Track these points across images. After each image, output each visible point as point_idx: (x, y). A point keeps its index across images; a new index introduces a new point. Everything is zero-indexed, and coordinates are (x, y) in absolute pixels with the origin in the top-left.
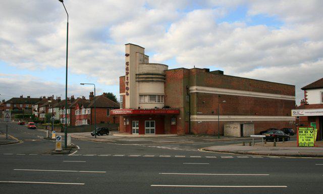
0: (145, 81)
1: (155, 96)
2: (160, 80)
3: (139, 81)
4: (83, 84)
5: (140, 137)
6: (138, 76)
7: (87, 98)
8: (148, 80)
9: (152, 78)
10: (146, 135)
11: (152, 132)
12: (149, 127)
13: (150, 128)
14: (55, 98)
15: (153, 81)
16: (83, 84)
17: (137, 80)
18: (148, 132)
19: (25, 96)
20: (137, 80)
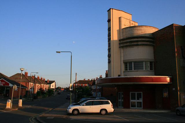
0: (129, 46)
1: (142, 62)
2: (148, 43)
3: (122, 47)
4: (59, 52)
5: (143, 114)
6: (122, 42)
7: (40, 78)
8: (133, 44)
9: (137, 41)
10: (132, 110)
11: (139, 105)
12: (138, 102)
13: (136, 101)
14: (99, 78)
15: (137, 45)
16: (59, 52)
17: (122, 45)
18: (134, 106)
19: (87, 79)
20: (122, 45)
